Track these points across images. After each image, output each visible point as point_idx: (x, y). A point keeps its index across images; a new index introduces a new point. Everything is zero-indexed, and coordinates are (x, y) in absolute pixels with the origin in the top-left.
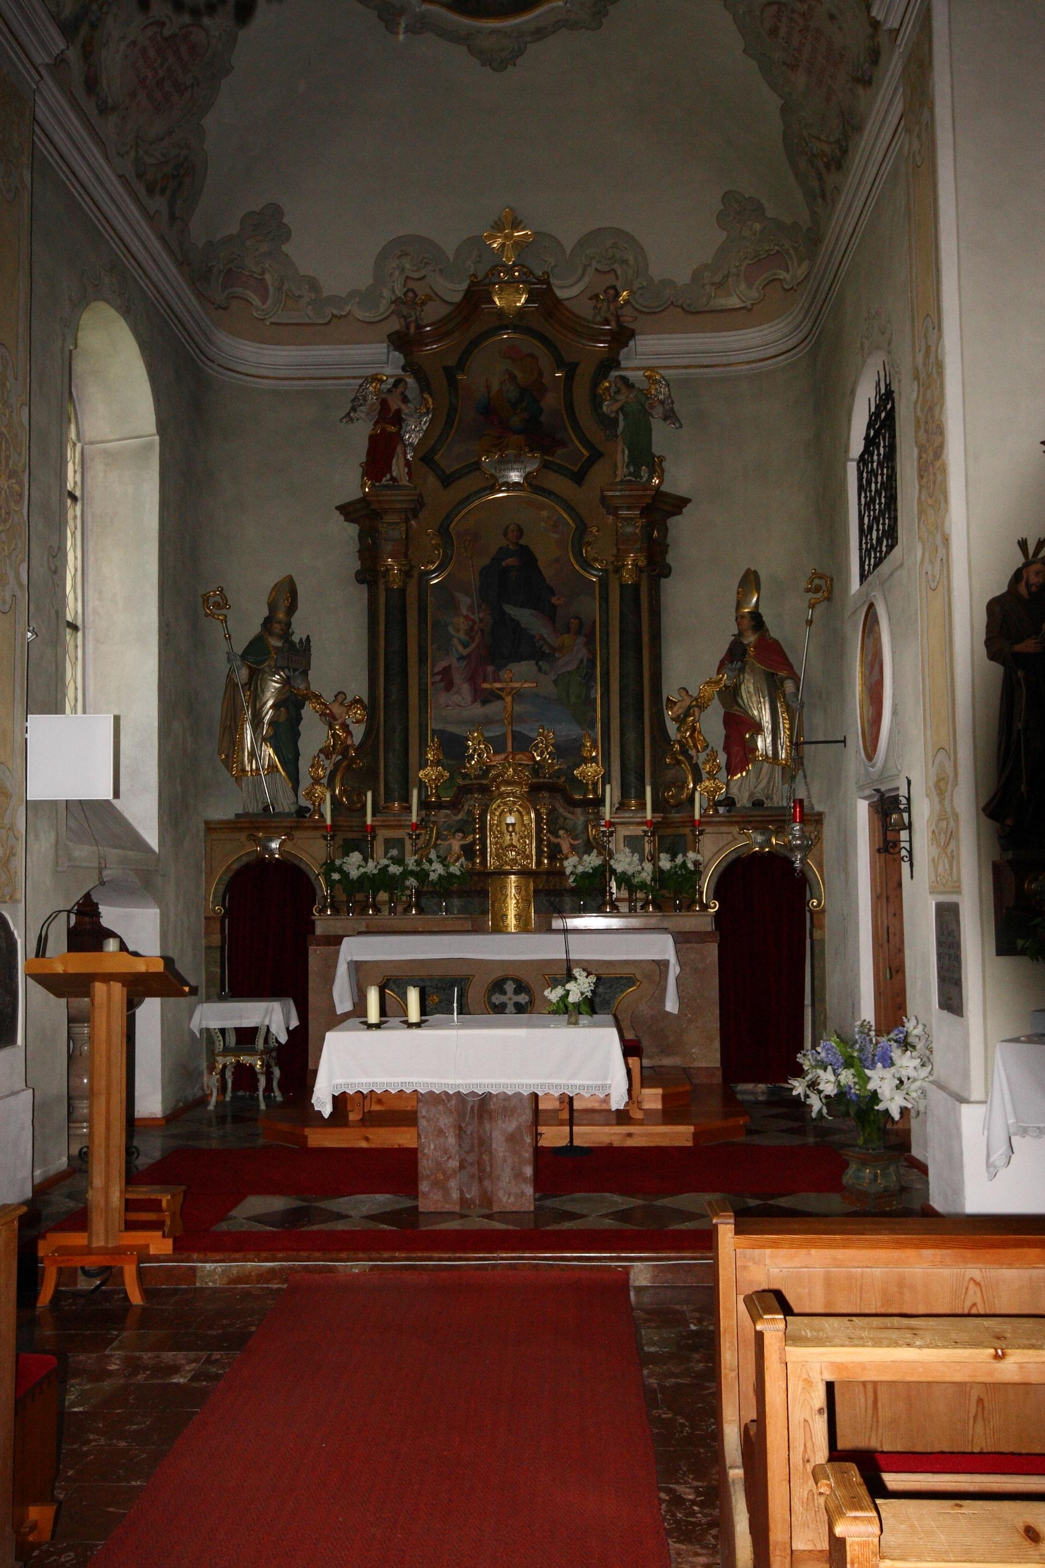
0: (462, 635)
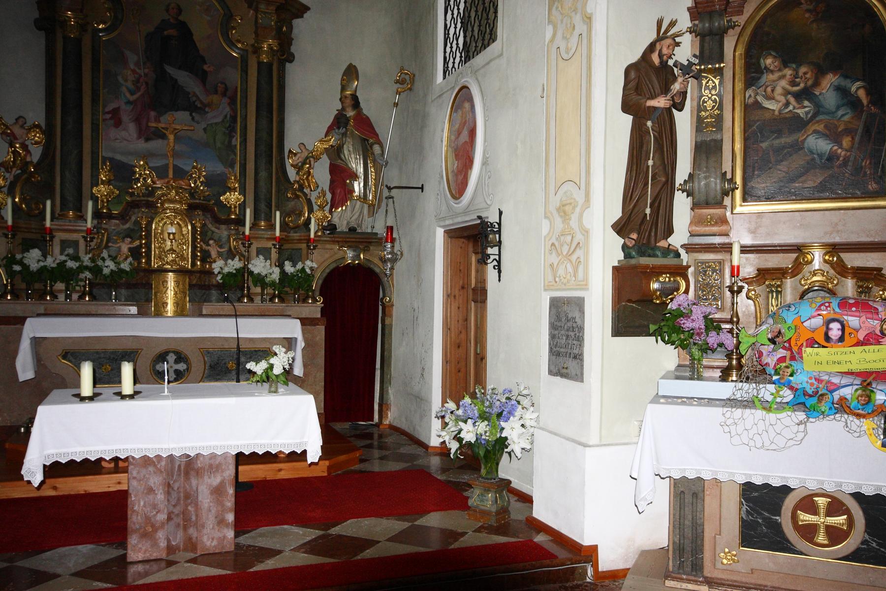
0: (129, 84)
